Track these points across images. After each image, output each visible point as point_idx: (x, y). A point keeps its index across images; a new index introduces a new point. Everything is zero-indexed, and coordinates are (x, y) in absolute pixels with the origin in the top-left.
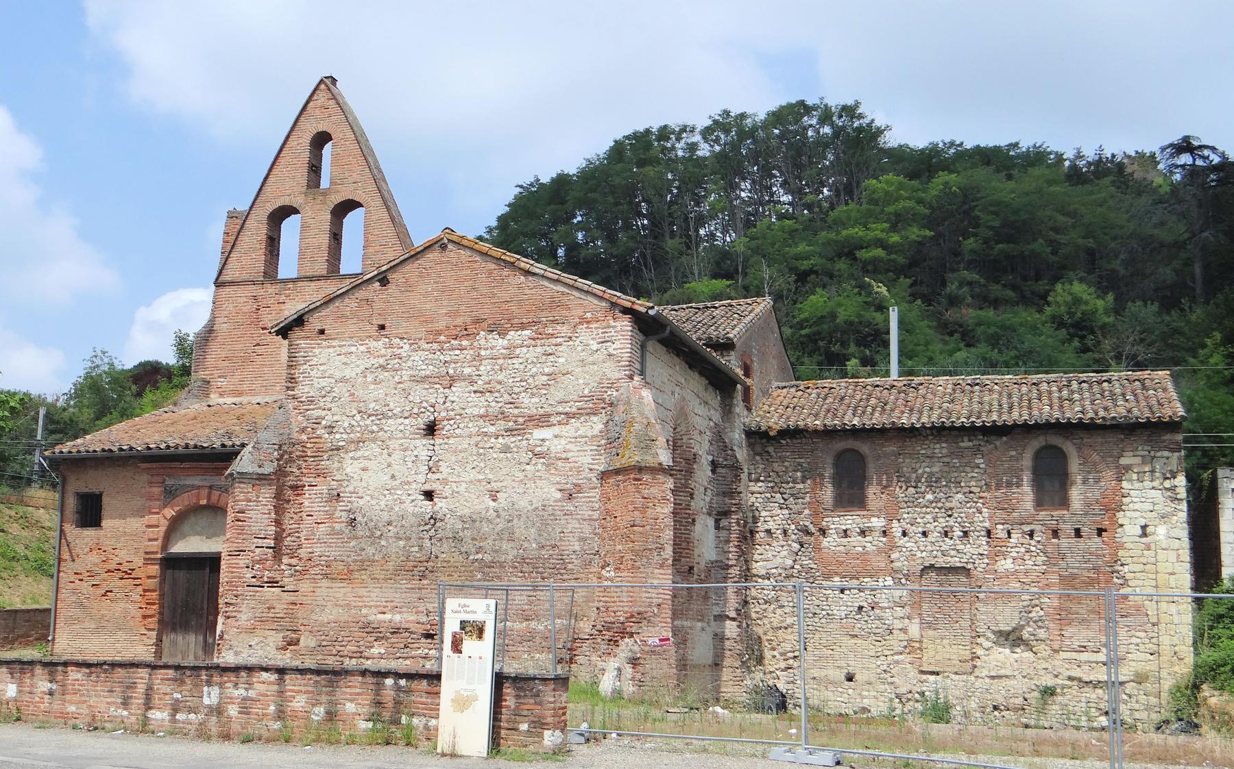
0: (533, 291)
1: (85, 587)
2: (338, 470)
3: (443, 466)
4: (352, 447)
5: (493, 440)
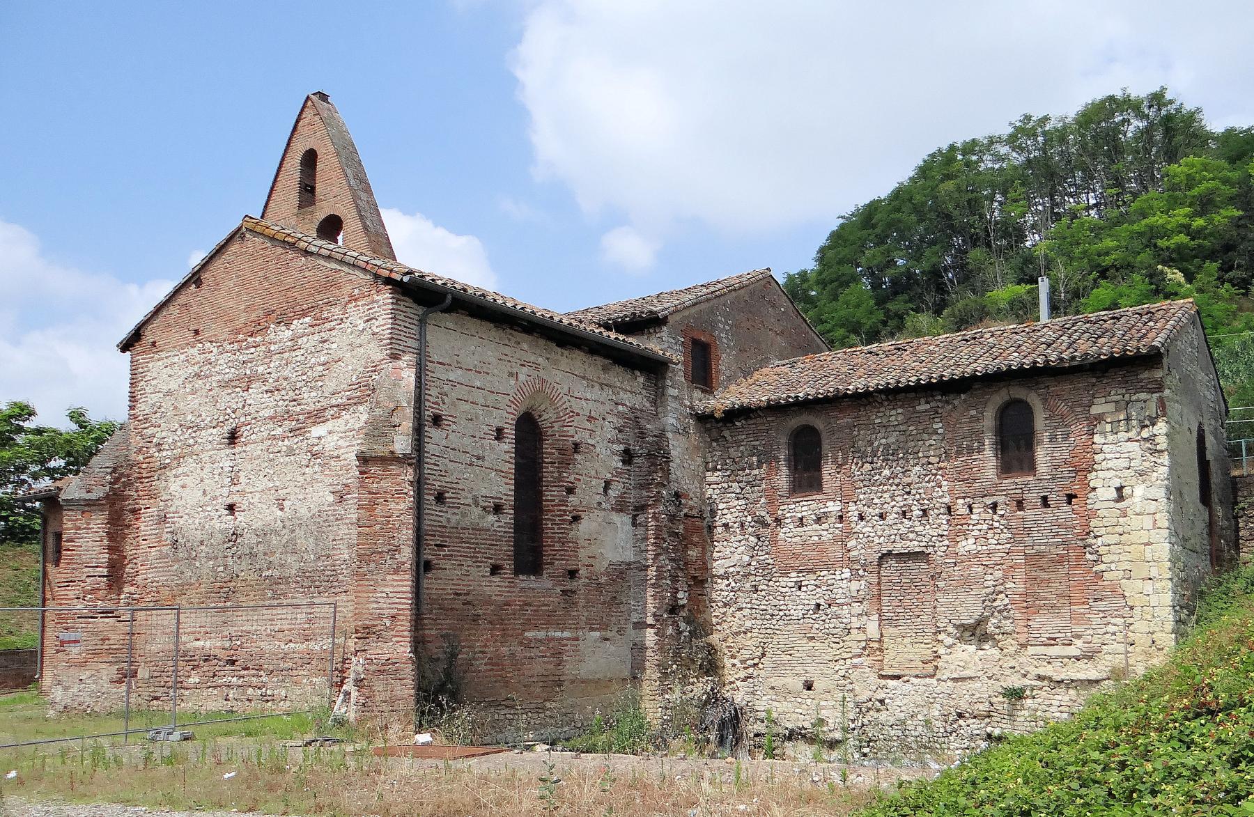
4: (175, 464)
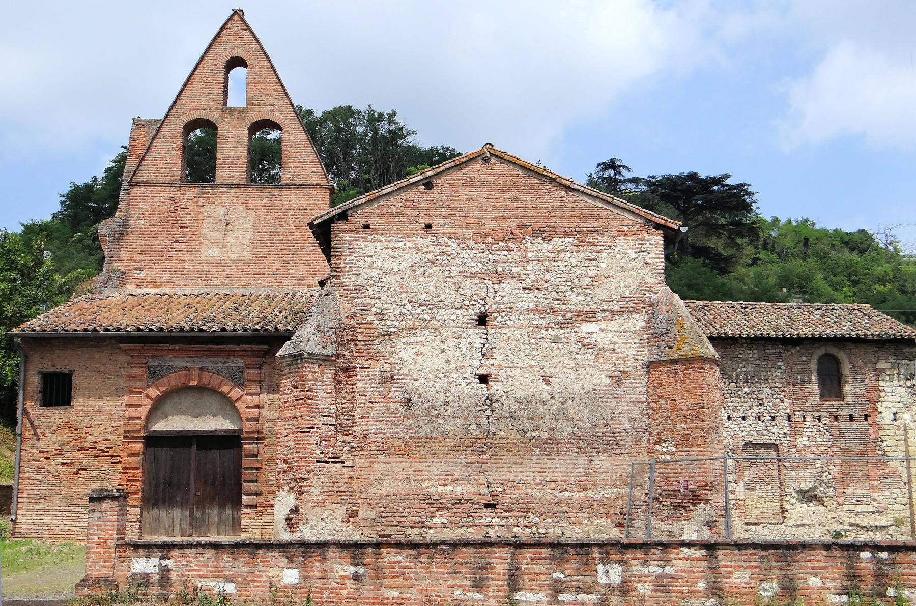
0: (574, 205)
1: (53, 465)
2: (391, 354)
3: (497, 354)
4: (405, 333)
5: (543, 331)
